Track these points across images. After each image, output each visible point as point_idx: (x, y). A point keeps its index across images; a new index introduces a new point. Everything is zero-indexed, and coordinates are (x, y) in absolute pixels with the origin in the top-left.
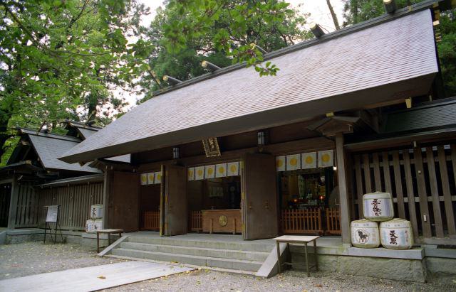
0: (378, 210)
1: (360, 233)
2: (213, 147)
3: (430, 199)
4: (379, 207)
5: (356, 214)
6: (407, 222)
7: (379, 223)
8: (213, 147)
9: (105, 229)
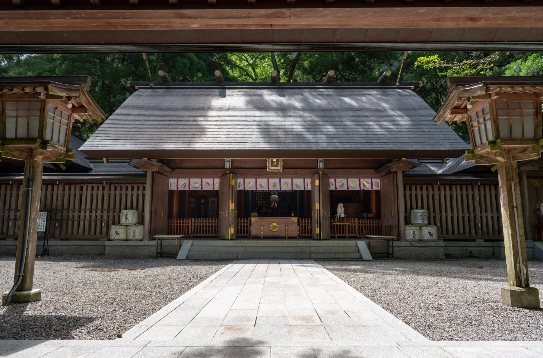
0: (127, 219)
1: (116, 232)
2: (275, 163)
3: (79, 214)
4: (128, 217)
5: (408, 222)
6: (435, 227)
7: (420, 227)
8: (275, 163)
9: (502, 258)
